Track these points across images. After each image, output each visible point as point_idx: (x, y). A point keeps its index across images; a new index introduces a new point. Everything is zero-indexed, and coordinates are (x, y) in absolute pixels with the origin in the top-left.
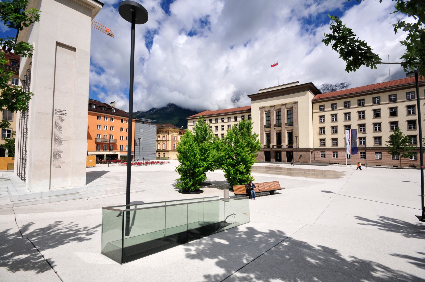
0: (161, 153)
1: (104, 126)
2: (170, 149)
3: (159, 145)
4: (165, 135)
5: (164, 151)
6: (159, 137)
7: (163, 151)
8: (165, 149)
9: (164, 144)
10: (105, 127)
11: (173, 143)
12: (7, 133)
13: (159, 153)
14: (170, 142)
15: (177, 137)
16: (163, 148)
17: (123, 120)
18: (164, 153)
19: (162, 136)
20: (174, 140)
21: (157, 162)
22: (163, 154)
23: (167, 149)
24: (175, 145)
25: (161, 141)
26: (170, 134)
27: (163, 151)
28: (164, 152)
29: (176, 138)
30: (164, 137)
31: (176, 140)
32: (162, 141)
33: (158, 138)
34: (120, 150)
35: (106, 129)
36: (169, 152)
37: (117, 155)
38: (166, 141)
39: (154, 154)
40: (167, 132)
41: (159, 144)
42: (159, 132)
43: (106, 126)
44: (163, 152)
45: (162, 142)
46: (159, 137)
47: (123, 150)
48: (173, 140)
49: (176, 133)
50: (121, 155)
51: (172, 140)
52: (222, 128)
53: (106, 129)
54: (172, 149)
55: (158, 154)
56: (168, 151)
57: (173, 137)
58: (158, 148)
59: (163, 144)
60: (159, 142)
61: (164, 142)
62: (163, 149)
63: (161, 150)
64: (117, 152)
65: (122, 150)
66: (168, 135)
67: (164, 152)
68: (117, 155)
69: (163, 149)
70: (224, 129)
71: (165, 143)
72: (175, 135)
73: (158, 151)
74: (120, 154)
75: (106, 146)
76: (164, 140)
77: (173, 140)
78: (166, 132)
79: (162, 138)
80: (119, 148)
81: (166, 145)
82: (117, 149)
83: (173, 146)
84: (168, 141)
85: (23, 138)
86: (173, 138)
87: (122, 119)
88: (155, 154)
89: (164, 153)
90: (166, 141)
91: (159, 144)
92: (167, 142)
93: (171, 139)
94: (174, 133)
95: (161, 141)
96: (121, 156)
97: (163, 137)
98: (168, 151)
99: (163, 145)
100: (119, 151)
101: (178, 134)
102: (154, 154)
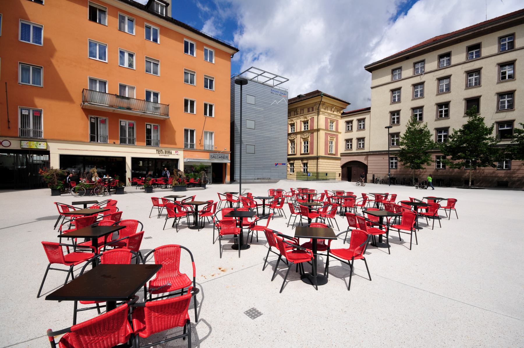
0: (298, 165)
1: (122, 53)
2: (322, 153)
3: (292, 145)
4: (309, 118)
5: (305, 159)
6: (292, 125)
7: (302, 159)
8: (308, 154)
9: (306, 141)
10: (126, 55)
11: (329, 138)
12: (135, 161)
13: (292, 165)
14: (322, 134)
15: (337, 121)
16: (303, 152)
17: (192, 45)
18: (305, 165)
19: (299, 121)
20: (330, 131)
21: (299, 189)
22: (302, 165)
23: (313, 153)
24: (332, 142)
25: (296, 133)
26: (324, 113)
27: (302, 159)
28: (305, 162)
29: (334, 124)
30: (306, 122)
31: (334, 129)
32: (301, 133)
33: (290, 127)
34: (186, 145)
35: (131, 65)
36: (320, 160)
37: (177, 160)
38: (312, 131)
39: (283, 164)
40: (313, 108)
41: (293, 142)
42: (292, 113)
43: (131, 55)
44: (302, 161)
45: (299, 136)
46: (292, 125)
47: (195, 147)
48: (329, 129)
49: (335, 113)
50: (185, 161)
51: (326, 129)
52: (348, 145)
53: (131, 65)
54: (325, 154)
55: (289, 165)
56: (317, 158)
57: (329, 121)
58: (290, 153)
59: (302, 140)
60: (292, 137)
61: (306, 135)
62: (301, 154)
63: (298, 155)
64: (173, 152)
65: (192, 146)
66: (318, 115)
67: (305, 162)
68: (176, 161)
69: (301, 154)
70: (351, 147)
71: (309, 139)
72: (332, 117)
73: (291, 160)
74: (184, 158)
75: (131, 127)
76: (304, 132)
77: (328, 130)
78: (311, 110)
79: (300, 126)
80: (180, 137)
81: (312, 143)
82: (174, 143)
83: (329, 145)
84: (318, 130)
85: (124, 122)
86: (329, 124)
87: (190, 42)
88: (285, 164)
89: (305, 165)
90: (312, 131)
91: (293, 142)
92: (315, 134)
93: (324, 127)
94: (332, 112)
95: (296, 133)
96: (186, 166)
97: (302, 123)
98: (317, 158)
99: (303, 143)
100: (180, 149)
101: (340, 114)
102: (283, 164)
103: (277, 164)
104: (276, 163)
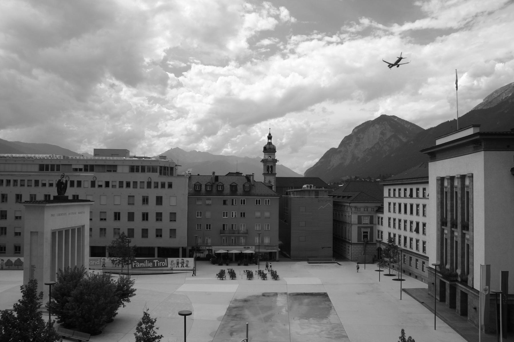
39: (328, 247)
102: (328, 247)
103: (324, 247)
104: (323, 247)
